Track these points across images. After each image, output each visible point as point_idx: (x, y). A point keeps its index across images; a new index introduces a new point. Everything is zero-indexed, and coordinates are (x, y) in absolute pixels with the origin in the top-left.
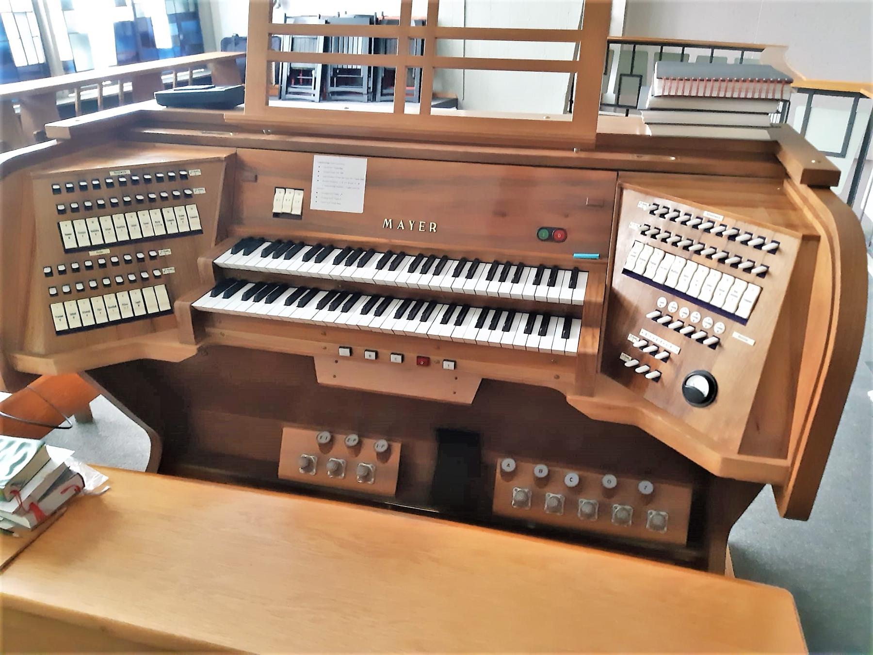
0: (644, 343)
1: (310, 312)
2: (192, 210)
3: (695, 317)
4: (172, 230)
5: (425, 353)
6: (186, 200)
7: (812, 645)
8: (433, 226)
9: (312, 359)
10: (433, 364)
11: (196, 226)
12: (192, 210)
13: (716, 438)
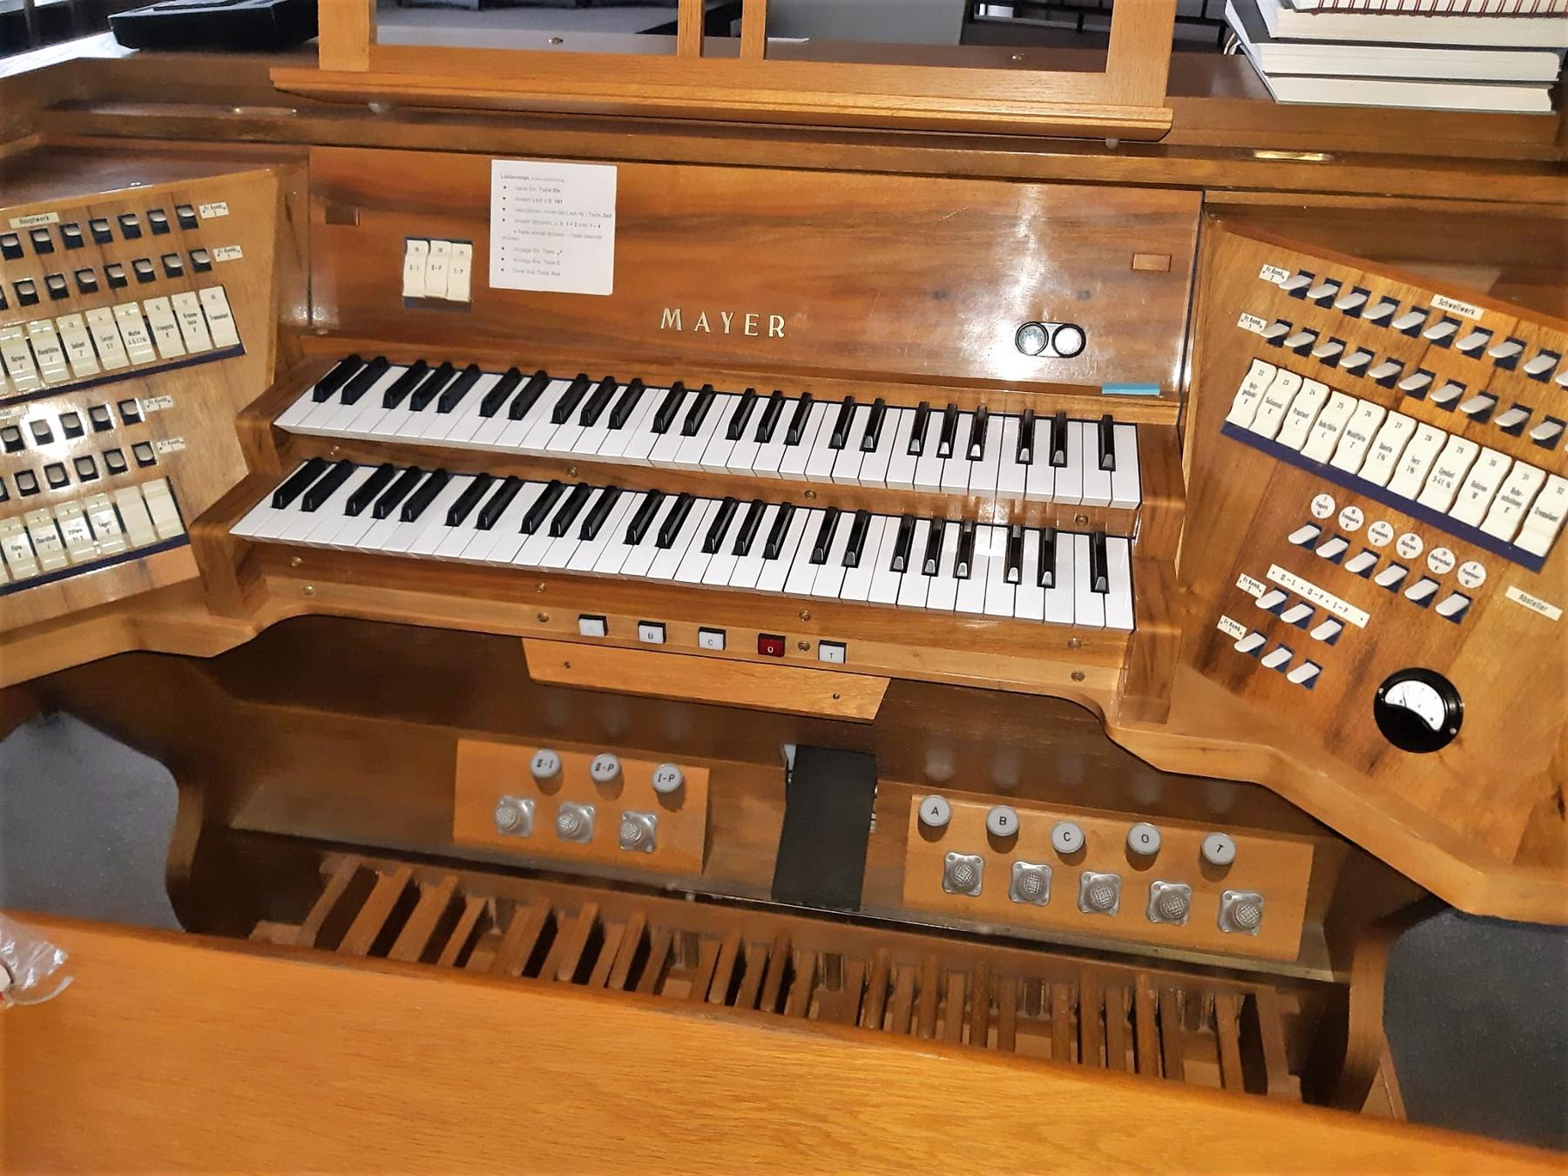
0: (1276, 598)
1: (504, 544)
2: (215, 299)
3: (1412, 546)
4: (171, 348)
5: (774, 625)
6: (201, 273)
7: (1545, 1129)
8: (777, 324)
9: (518, 640)
10: (792, 652)
11: (226, 335)
12: (215, 299)
13: (1458, 825)
